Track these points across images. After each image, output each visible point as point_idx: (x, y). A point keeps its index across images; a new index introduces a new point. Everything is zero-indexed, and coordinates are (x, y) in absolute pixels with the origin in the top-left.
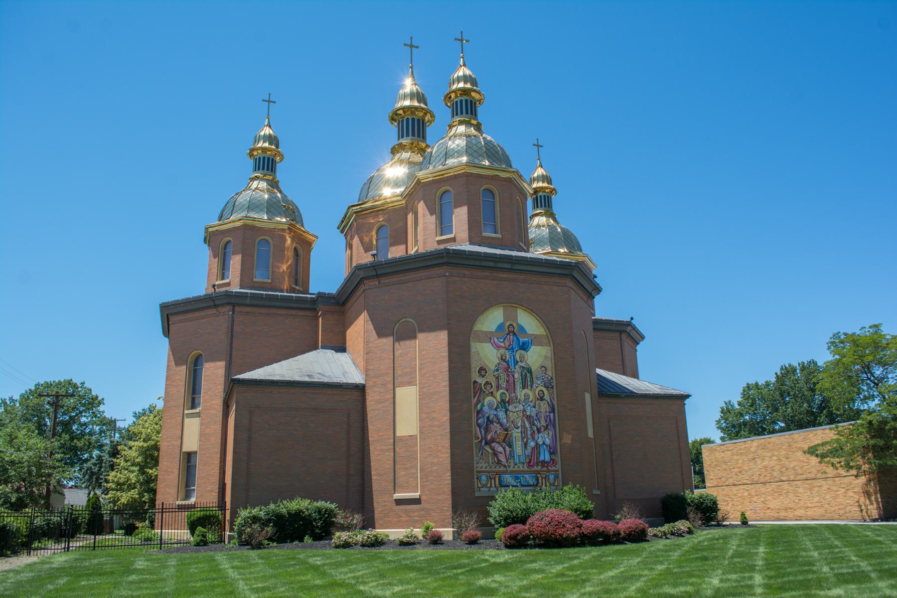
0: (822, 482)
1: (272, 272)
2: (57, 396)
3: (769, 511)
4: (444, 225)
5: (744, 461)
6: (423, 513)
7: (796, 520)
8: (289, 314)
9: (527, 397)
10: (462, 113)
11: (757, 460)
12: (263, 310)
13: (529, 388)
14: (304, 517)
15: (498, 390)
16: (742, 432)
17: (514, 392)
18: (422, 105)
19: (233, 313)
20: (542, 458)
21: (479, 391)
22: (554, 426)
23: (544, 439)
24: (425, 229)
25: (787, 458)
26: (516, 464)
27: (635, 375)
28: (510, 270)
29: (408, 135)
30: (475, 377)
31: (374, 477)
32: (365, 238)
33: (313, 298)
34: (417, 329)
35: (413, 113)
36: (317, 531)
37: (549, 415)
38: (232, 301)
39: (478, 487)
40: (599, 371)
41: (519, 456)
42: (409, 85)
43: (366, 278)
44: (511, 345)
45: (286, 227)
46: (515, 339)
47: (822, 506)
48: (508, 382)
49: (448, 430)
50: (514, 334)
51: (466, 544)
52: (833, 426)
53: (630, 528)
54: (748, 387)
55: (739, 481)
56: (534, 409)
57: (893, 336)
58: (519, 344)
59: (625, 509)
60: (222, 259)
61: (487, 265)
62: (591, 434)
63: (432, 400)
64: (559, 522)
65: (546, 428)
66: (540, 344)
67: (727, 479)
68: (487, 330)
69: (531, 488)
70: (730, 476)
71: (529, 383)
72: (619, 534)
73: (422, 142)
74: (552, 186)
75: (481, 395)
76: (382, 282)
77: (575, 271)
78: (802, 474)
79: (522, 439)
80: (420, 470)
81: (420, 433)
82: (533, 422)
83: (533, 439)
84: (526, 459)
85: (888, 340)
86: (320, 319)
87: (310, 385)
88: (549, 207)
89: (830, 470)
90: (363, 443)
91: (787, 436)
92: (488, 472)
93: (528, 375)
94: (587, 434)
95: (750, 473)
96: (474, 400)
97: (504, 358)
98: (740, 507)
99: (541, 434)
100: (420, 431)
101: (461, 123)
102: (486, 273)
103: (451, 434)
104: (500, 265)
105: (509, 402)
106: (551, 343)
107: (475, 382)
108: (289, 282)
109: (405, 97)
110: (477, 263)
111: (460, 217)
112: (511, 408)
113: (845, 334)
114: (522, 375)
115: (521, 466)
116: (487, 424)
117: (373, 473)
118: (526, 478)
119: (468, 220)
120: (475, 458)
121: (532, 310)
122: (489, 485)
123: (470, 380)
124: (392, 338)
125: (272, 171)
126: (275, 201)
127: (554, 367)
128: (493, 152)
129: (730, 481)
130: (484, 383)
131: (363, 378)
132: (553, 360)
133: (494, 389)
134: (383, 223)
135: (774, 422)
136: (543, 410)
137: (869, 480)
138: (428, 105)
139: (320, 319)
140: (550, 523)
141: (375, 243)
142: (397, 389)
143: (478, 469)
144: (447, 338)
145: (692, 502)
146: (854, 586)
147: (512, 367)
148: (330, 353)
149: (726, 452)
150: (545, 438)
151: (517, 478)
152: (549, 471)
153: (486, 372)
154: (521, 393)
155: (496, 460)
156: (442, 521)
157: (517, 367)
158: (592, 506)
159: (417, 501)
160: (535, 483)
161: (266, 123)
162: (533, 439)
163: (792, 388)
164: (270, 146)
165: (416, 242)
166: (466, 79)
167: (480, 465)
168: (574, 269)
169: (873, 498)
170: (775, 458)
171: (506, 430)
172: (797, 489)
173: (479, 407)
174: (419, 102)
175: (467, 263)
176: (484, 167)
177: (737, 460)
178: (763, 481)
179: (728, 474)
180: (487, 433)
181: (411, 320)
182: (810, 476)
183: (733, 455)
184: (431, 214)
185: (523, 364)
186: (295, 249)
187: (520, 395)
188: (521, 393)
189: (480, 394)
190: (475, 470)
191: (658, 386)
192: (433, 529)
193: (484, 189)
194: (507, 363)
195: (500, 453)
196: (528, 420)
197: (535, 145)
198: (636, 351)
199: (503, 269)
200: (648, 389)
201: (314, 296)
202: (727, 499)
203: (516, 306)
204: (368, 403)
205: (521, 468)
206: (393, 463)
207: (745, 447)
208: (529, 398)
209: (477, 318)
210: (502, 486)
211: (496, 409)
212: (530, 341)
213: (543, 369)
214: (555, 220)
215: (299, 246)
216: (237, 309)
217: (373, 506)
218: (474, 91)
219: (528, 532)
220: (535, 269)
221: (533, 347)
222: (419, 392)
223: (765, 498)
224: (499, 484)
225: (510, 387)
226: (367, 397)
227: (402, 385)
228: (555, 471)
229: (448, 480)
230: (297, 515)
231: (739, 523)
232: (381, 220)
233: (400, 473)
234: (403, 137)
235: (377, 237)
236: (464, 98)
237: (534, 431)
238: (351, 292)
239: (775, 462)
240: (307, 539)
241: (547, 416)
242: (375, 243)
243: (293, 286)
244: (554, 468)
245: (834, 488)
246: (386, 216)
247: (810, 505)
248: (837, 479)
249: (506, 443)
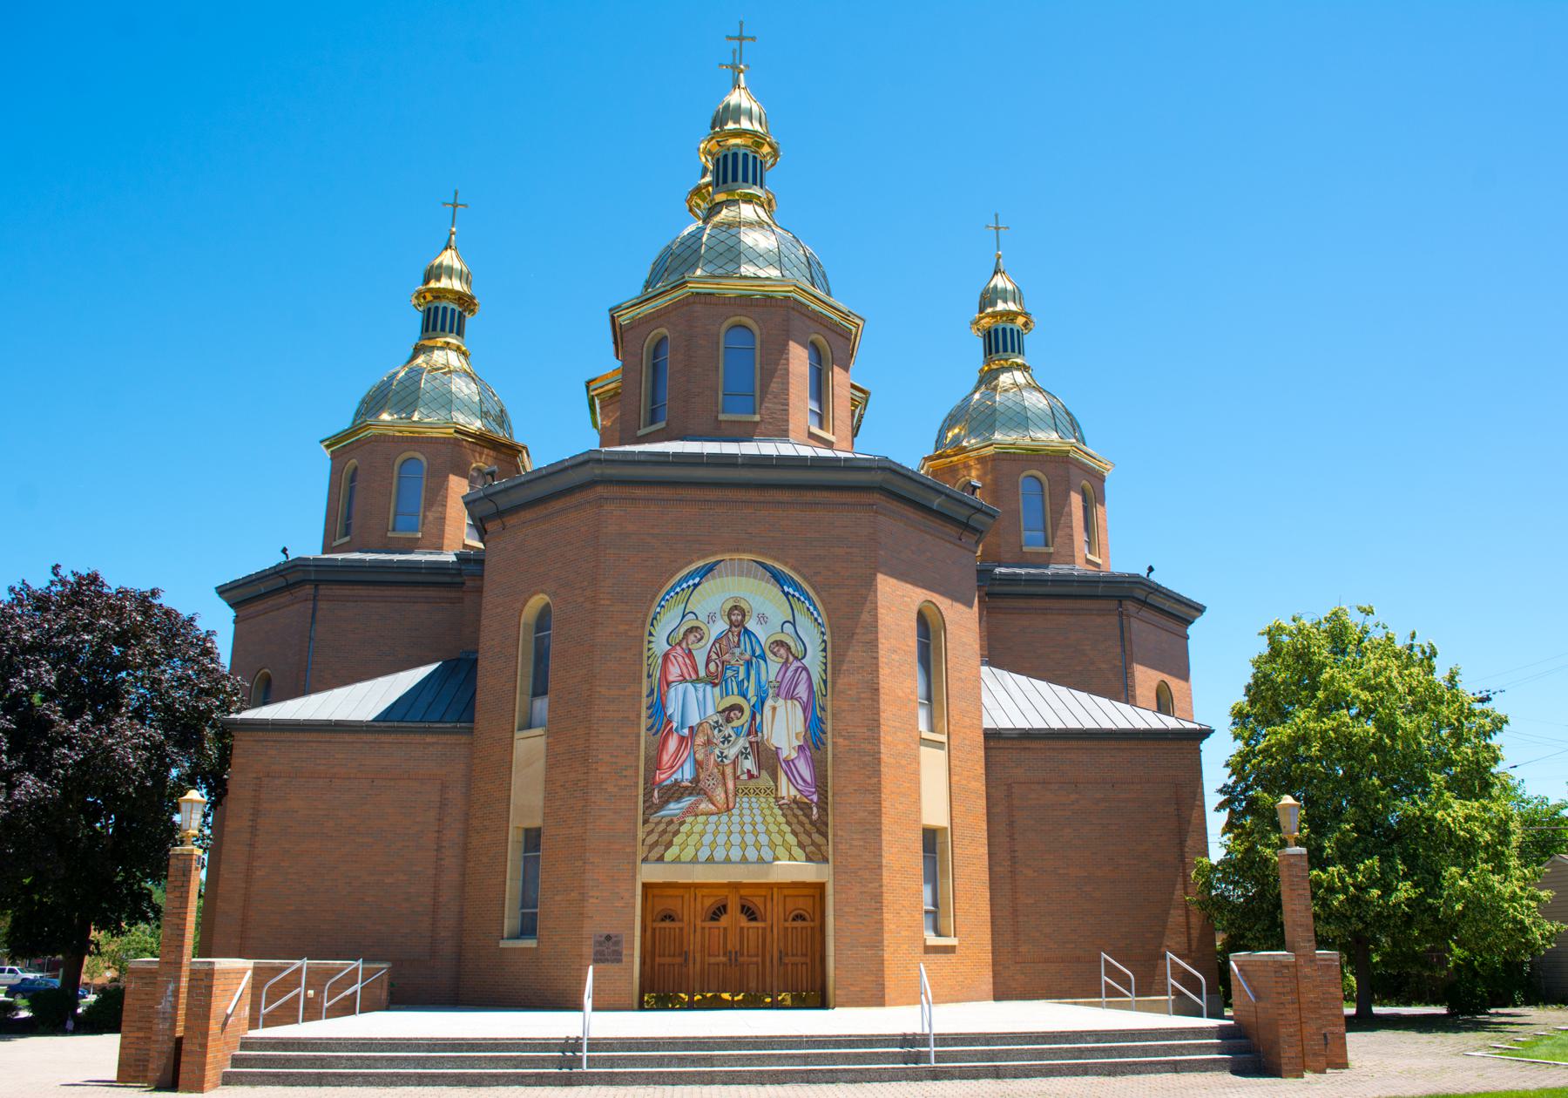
198: (1187, 637)
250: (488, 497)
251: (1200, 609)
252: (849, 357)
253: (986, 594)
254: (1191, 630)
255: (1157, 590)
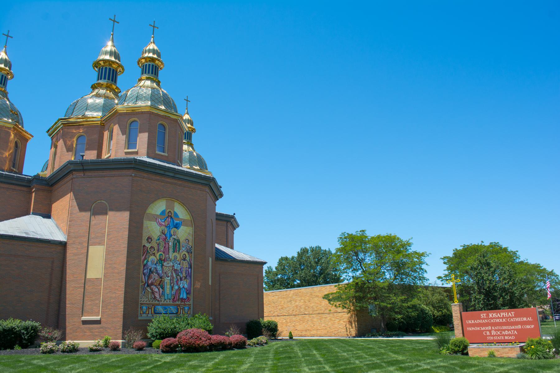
0: (327, 315)
3: (296, 331)
4: (131, 143)
6: (102, 330)
7: (311, 336)
9: (175, 258)
10: (149, 73)
11: (292, 301)
13: (178, 252)
14: (15, 332)
15: (158, 252)
16: (276, 285)
17: (168, 254)
18: (117, 61)
20: (181, 296)
21: (146, 252)
22: (191, 277)
23: (183, 285)
24: (117, 143)
25: (309, 301)
26: (165, 300)
27: (232, 248)
28: (173, 177)
29: (105, 79)
30: (144, 242)
32: (68, 142)
33: (29, 179)
34: (108, 208)
35: (110, 65)
36: (24, 342)
37: (188, 270)
40: (217, 246)
41: (168, 294)
42: (109, 46)
43: (74, 170)
45: (12, 126)
46: (171, 221)
47: (326, 329)
48: (165, 247)
49: (124, 276)
50: (171, 218)
51: (136, 350)
52: (337, 284)
53: (237, 340)
54: (282, 259)
55: (281, 314)
56: (179, 265)
57: (372, 237)
58: (174, 224)
59: (231, 329)
61: (159, 173)
62: (210, 283)
63: (115, 255)
64: (197, 337)
65: (186, 278)
66: (186, 225)
67: (274, 312)
68: (154, 213)
69: (175, 315)
71: (178, 249)
72: (231, 344)
73: (114, 84)
74: (194, 127)
76: (86, 174)
77: (212, 183)
78: (317, 311)
79: (170, 284)
80: (102, 301)
81: (104, 277)
82: (178, 274)
83: (177, 284)
84: (172, 297)
85: (369, 239)
86: (34, 194)
88: (190, 139)
89: (333, 309)
90: (61, 282)
91: (310, 289)
92: (148, 304)
93: (178, 244)
94: (209, 283)
95: (287, 309)
96: (143, 258)
97: (163, 232)
100: (104, 275)
101: (148, 79)
102: (158, 178)
103: (126, 279)
104: (167, 173)
105: (164, 260)
106: (193, 225)
107: (144, 246)
108: (9, 165)
109: (106, 53)
110: (153, 170)
111: (143, 139)
112: (165, 264)
113: (348, 234)
114: (174, 244)
115: (168, 301)
116: (149, 273)
117: (67, 302)
118: (171, 309)
119: (148, 142)
120: (140, 295)
121: (183, 203)
122: (147, 313)
123: (142, 244)
125: (4, 85)
126: (5, 106)
127: (193, 240)
128: (166, 101)
129: (276, 314)
130: (150, 247)
131: (65, 238)
132: (193, 236)
133: (155, 252)
134: (82, 134)
135: (294, 281)
136: (185, 267)
137: (352, 316)
138: (121, 61)
139: (34, 194)
140: (192, 337)
141: (75, 146)
142: (90, 246)
143: (141, 302)
144: (129, 216)
145: (264, 325)
146: (378, 370)
148: (39, 218)
149: (275, 297)
150: (184, 284)
151: (165, 308)
152: (185, 305)
153: (152, 240)
154: (172, 255)
155: (153, 296)
156: (115, 335)
157: (171, 238)
158: (213, 327)
159: (98, 322)
161: (186, 112)
162: (177, 284)
163: (306, 261)
164: (5, 67)
165: (109, 150)
166: (154, 52)
168: (212, 182)
169: (354, 325)
170: (302, 301)
171: (161, 278)
172: (313, 319)
173: (145, 262)
174: (115, 58)
175: (142, 168)
176: (161, 110)
177: (281, 301)
178: (294, 314)
180: (149, 279)
181: (104, 202)
182: (321, 312)
183: (279, 298)
184: (123, 134)
185: (175, 237)
186: (16, 143)
188: (172, 255)
189: (147, 254)
190: (140, 302)
191: (249, 256)
192: (110, 341)
193: (159, 124)
194: (165, 235)
195: (156, 292)
196: (175, 272)
197: (185, 100)
198: (234, 233)
200: (243, 257)
201: (30, 178)
203: (175, 200)
205: (168, 302)
206: (82, 296)
207: (286, 294)
208: (177, 259)
209: (149, 205)
210: (155, 313)
211: (156, 264)
213: (187, 241)
214: (193, 148)
215: (19, 140)
217: (66, 325)
218: (159, 60)
219: (177, 342)
220: (188, 178)
221: (182, 227)
222: (106, 250)
223: (295, 324)
224: (154, 312)
225: (166, 251)
226: (67, 251)
227: (95, 244)
228: (188, 305)
229: (121, 308)
230: (11, 331)
231: (288, 338)
232: (81, 131)
233: (88, 303)
234: (101, 79)
235: (77, 142)
236: (151, 63)
237: (178, 280)
238: (59, 180)
239: (302, 303)
240: (17, 348)
241: (187, 270)
242: (75, 146)
243: (12, 168)
244: (188, 303)
245: (333, 319)
246: (85, 130)
247: (319, 328)
248: (335, 314)
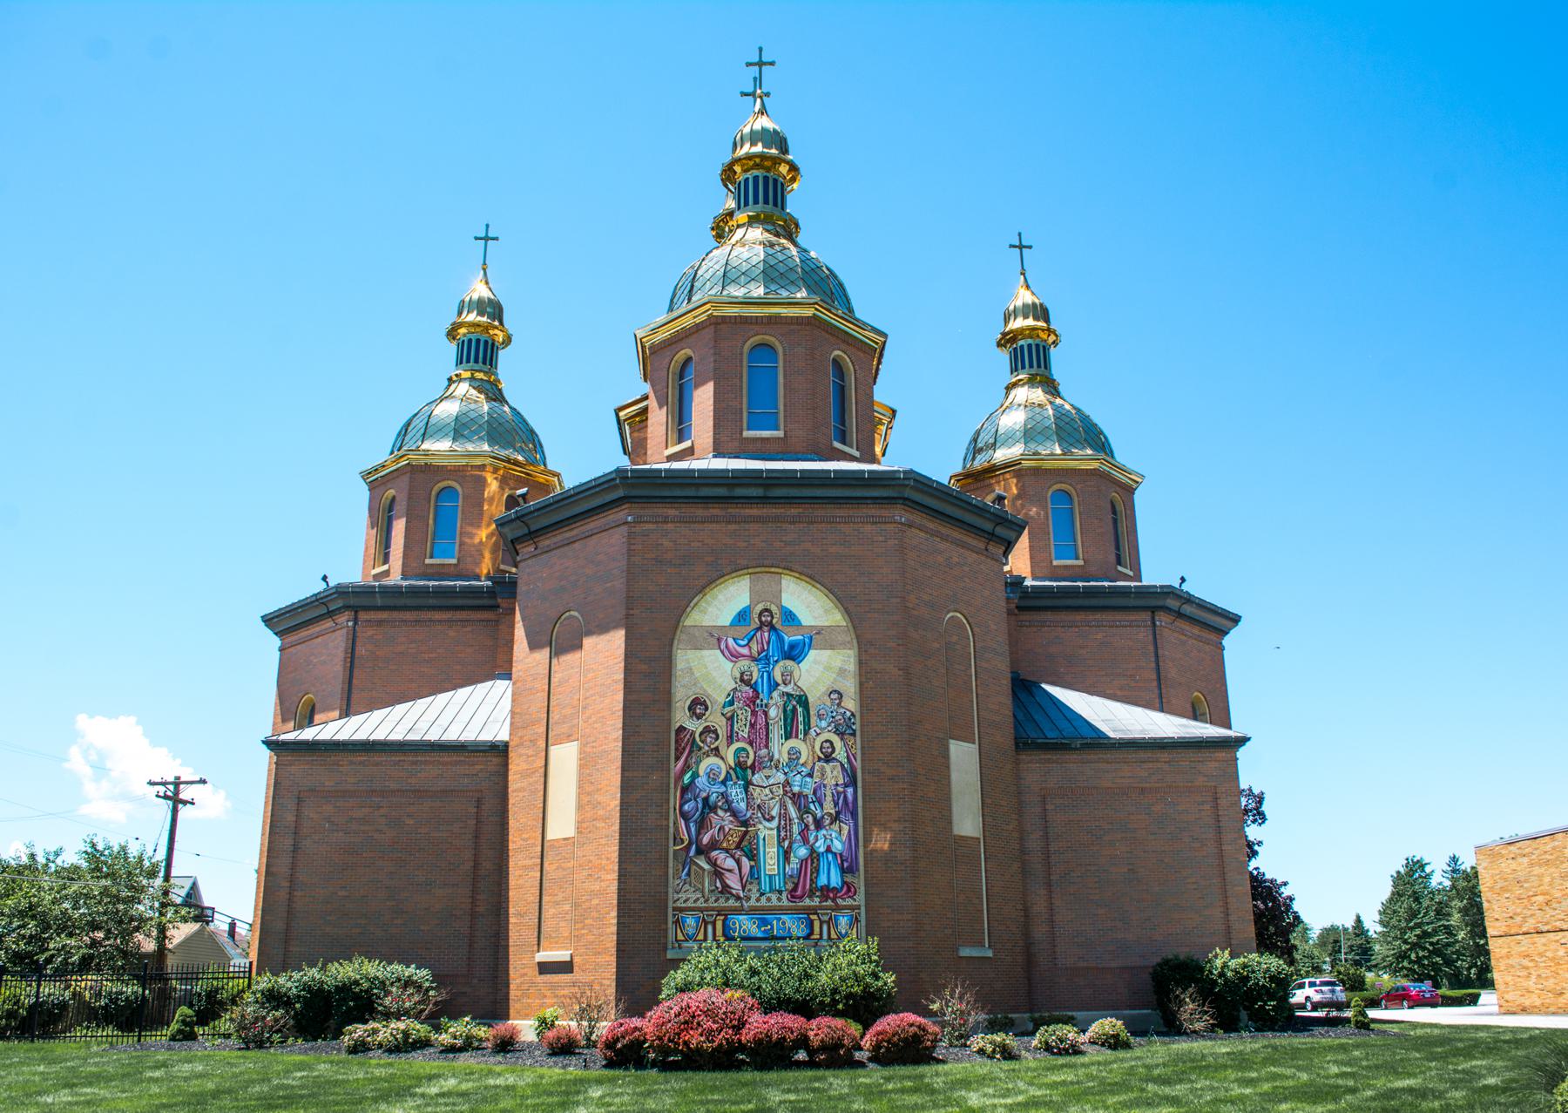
1: (460, 545)
2: (177, 783)
5: (1553, 879)
8: (454, 618)
9: (794, 755)
12: (408, 615)
13: (801, 736)
17: (767, 746)
19: (355, 624)
20: (822, 881)
21: (687, 745)
22: (854, 815)
26: (762, 894)
28: (764, 500)
30: (681, 717)
31: (512, 920)
37: (845, 792)
38: (352, 601)
39: (676, 940)
41: (770, 876)
44: (763, 650)
46: (774, 638)
48: (752, 726)
49: (617, 827)
55: (1547, 924)
56: (808, 779)
58: (783, 647)
60: (385, 529)
65: (836, 818)
67: (1525, 919)
68: (711, 624)
70: (1529, 913)
71: (801, 727)
75: (693, 754)
79: (779, 842)
83: (805, 840)
84: (785, 883)
87: (406, 748)
92: (701, 910)
93: (800, 710)
97: (746, 678)
98: (1552, 981)
99: (824, 832)
104: (739, 492)
105: (753, 767)
107: (681, 729)
108: (494, 560)
110: (691, 492)
114: (785, 711)
115: (774, 897)
116: (702, 812)
117: (512, 911)
121: (812, 574)
122: (701, 937)
124: (547, 650)
129: (1530, 925)
130: (700, 729)
136: (830, 782)
144: (623, 645)
147: (764, 695)
149: (1520, 860)
150: (835, 839)
151: (764, 922)
152: (838, 908)
153: (707, 709)
154: (780, 748)
155: (718, 884)
157: (775, 694)
160: (807, 931)
162: (805, 840)
167: (683, 896)
171: (745, 823)
173: (687, 779)
177: (1540, 876)
179: (1525, 907)
180: (702, 831)
185: (789, 689)
187: (780, 752)
188: (780, 748)
189: (691, 752)
190: (670, 904)
194: (754, 687)
196: (794, 803)
198: (1223, 649)
199: (748, 500)
202: (1526, 962)
203: (780, 571)
204: (512, 777)
205: (775, 902)
207: (1554, 848)
208: (798, 758)
211: (724, 783)
212: (807, 640)
213: (834, 696)
216: (363, 616)
217: (508, 974)
221: (812, 653)
224: (724, 935)
225: (759, 736)
228: (852, 908)
237: (807, 826)
241: (838, 793)
244: (849, 902)
249: (742, 850)
250: (519, 518)
251: (1235, 619)
252: (871, 381)
253: (1017, 607)
254: (1226, 641)
255: (1189, 599)
